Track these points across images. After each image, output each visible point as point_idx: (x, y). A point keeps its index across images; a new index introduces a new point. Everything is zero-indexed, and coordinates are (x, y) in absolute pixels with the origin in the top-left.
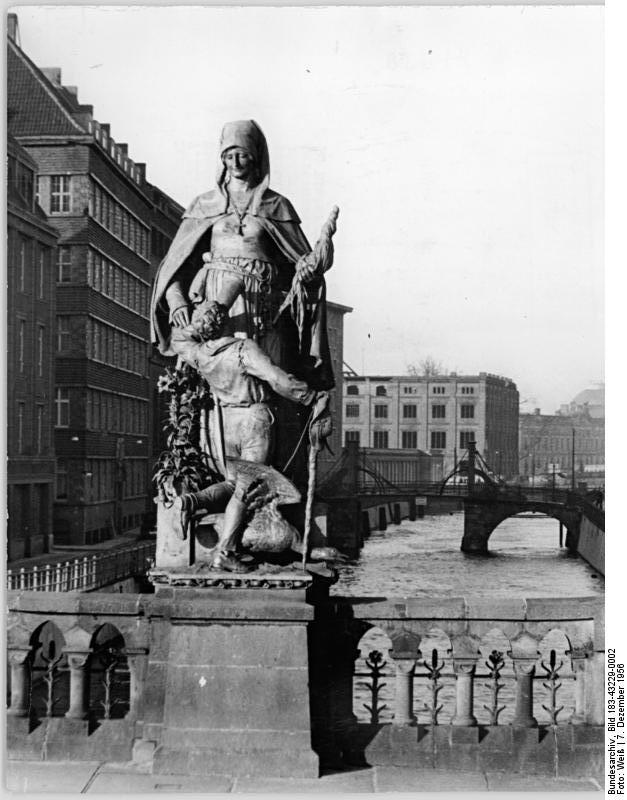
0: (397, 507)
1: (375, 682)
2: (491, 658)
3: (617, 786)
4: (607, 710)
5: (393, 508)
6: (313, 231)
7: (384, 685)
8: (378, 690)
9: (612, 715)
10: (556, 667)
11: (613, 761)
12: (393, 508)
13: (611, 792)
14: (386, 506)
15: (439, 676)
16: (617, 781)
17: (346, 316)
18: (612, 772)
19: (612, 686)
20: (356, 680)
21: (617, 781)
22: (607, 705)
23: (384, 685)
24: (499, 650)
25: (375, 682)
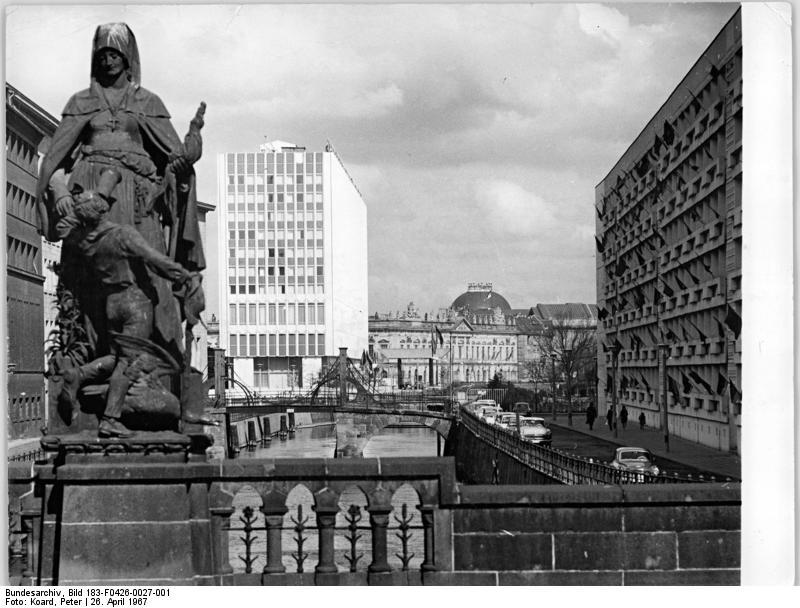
0: (266, 421)
1: (248, 536)
2: (349, 511)
3: (14, 598)
4: (90, 588)
5: (262, 422)
6: (181, 126)
7: (256, 537)
8: (407, 539)
9: (85, 593)
10: (407, 519)
11: (39, 594)
12: (262, 422)
13: (8, 592)
14: (254, 420)
15: (408, 527)
16: (19, 598)
17: (208, 215)
18: (28, 593)
19: (144, 593)
20: (388, 531)
21: (19, 598)
22: (95, 588)
23: (256, 537)
24: (355, 504)
25: (248, 536)
